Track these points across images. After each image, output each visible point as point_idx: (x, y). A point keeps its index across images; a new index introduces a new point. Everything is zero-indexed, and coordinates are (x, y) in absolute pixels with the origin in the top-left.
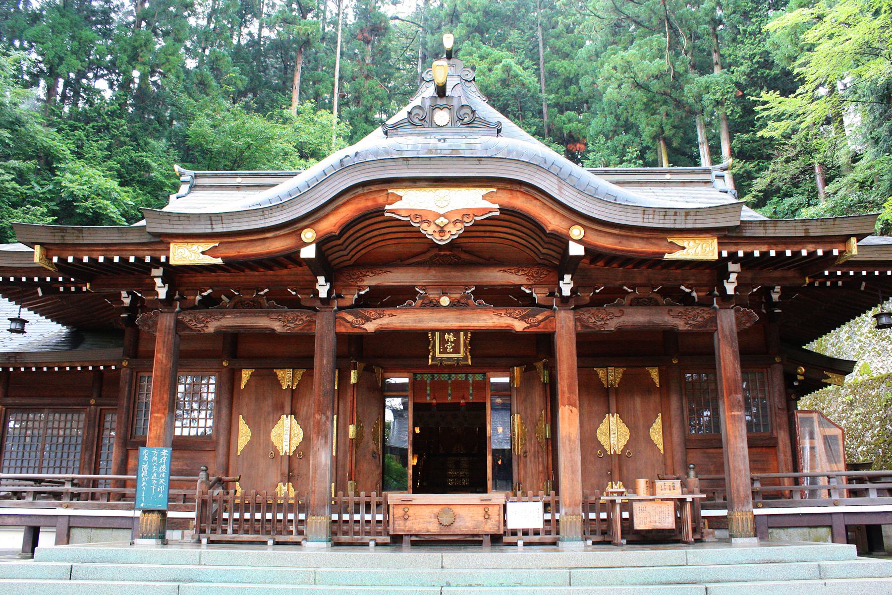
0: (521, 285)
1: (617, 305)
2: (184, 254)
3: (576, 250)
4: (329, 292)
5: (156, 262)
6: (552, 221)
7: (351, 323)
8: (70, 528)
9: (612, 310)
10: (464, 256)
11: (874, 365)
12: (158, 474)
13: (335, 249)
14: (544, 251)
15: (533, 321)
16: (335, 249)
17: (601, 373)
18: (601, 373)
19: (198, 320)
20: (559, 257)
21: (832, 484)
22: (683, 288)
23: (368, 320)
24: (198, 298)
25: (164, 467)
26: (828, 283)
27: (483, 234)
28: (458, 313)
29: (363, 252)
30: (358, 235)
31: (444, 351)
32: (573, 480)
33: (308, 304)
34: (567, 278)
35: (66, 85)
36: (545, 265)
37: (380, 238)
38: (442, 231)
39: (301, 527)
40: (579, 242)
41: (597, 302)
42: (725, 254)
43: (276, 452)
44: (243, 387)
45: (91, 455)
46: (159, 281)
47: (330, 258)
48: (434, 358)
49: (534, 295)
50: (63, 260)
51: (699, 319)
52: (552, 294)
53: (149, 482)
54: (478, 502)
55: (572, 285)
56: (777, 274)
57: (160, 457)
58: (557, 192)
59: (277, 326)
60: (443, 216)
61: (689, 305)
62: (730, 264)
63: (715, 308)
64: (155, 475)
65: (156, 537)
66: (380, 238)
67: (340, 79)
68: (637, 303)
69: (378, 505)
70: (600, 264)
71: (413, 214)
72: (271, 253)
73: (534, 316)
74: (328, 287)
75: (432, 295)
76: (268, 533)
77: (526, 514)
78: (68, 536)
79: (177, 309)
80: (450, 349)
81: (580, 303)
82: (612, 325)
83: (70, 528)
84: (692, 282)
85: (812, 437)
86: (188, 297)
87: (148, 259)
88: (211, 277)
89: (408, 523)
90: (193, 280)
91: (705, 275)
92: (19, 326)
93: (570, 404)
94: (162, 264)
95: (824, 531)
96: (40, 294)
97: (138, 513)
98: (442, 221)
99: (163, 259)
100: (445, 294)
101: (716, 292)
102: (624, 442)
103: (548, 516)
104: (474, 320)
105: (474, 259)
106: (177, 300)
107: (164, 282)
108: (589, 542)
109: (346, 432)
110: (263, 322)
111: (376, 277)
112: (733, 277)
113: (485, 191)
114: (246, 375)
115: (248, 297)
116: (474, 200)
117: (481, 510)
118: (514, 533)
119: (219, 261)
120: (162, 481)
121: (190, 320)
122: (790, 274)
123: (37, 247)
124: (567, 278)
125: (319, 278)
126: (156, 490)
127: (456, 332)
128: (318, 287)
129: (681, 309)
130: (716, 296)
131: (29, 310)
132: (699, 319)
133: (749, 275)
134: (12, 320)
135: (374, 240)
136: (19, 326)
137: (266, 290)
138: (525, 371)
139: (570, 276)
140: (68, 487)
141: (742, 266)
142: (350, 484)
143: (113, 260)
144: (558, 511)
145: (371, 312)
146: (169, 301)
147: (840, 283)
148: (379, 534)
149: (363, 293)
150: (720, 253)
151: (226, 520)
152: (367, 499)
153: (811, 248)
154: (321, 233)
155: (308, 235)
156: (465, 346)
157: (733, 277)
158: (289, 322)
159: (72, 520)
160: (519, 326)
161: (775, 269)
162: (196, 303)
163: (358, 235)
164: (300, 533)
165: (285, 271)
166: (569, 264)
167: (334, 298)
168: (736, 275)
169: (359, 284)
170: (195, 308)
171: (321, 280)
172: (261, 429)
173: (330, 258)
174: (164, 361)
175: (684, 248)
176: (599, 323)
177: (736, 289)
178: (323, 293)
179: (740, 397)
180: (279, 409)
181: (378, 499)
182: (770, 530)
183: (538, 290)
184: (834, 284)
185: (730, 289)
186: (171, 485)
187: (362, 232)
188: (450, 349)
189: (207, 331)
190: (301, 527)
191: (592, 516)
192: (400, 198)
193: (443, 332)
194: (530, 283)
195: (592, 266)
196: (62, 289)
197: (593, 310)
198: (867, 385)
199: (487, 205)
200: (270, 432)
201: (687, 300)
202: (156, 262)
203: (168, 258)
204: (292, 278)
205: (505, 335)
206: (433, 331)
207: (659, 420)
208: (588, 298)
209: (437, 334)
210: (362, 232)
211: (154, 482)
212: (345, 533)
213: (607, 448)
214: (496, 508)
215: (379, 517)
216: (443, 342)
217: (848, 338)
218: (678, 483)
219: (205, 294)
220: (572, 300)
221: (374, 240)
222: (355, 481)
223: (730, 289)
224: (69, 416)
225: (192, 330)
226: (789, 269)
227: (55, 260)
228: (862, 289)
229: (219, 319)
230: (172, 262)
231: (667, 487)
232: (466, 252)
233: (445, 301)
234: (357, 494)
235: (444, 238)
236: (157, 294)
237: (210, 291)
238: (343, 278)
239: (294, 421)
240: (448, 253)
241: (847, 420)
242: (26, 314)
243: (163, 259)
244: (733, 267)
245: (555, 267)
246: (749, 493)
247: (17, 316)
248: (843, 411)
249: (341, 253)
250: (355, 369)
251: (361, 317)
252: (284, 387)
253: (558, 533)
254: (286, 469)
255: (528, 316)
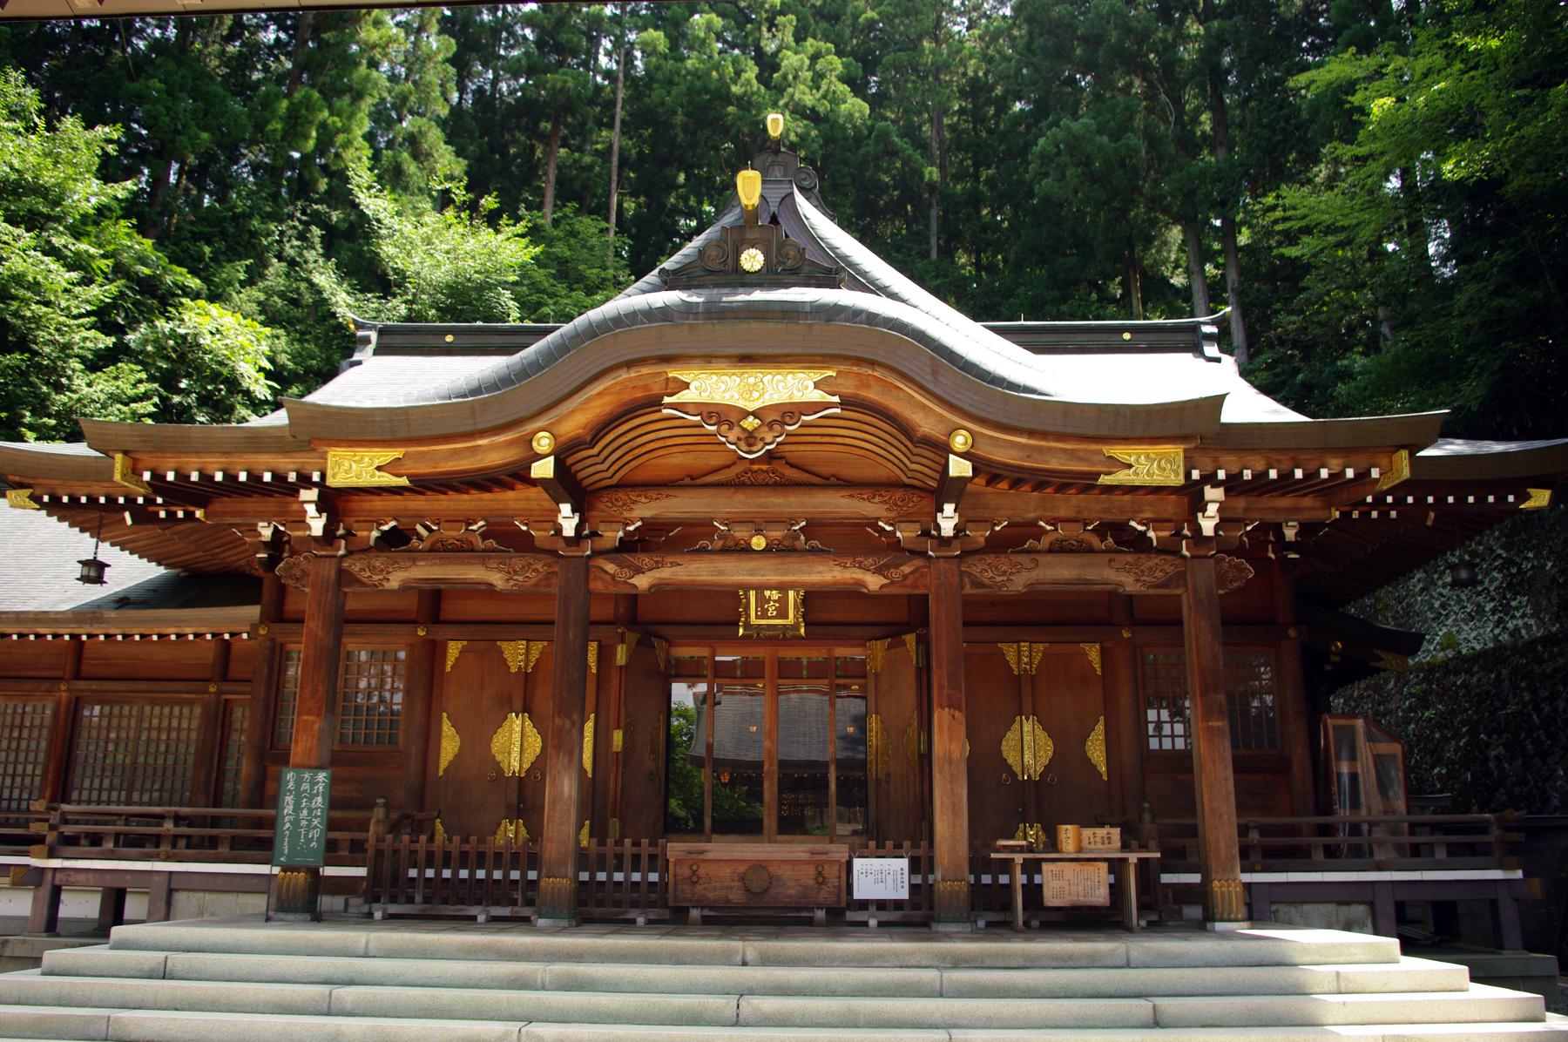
0: (878, 519)
1: (1028, 551)
2: (353, 468)
3: (959, 468)
4: (579, 528)
5: (304, 481)
6: (922, 423)
7: (613, 576)
8: (170, 892)
9: (1021, 558)
10: (791, 473)
11: (1464, 635)
12: (310, 811)
13: (588, 462)
14: (914, 467)
15: (895, 574)
16: (588, 462)
17: (1010, 652)
18: (1010, 652)
19: (373, 569)
20: (937, 476)
21: (1375, 836)
22: (1133, 523)
23: (639, 571)
24: (375, 534)
25: (320, 799)
26: (1374, 514)
27: (818, 439)
28: (778, 561)
29: (633, 464)
30: (623, 440)
31: (764, 615)
32: (954, 825)
33: (547, 546)
34: (949, 508)
35: (180, 173)
36: (915, 487)
37: (659, 444)
38: (750, 438)
39: (530, 894)
40: (964, 455)
41: (997, 545)
42: (1196, 475)
43: (500, 771)
44: (448, 669)
45: (210, 773)
46: (311, 509)
47: (581, 475)
48: (747, 626)
49: (899, 534)
50: (158, 477)
51: (1159, 574)
52: (926, 533)
53: (296, 823)
54: (805, 856)
55: (956, 520)
56: (1286, 502)
57: (313, 783)
58: (929, 377)
59: (497, 579)
60: (755, 414)
61: (1143, 552)
62: (1207, 489)
63: (1184, 557)
64: (305, 812)
65: (305, 911)
66: (659, 444)
67: (621, 166)
68: (1059, 548)
69: (653, 857)
70: (1003, 485)
71: (706, 410)
72: (485, 469)
73: (897, 566)
74: (576, 519)
75: (740, 533)
76: (478, 902)
77: (881, 877)
78: (169, 903)
79: (341, 552)
80: (772, 612)
81: (968, 548)
82: (1019, 582)
83: (170, 892)
84: (1148, 515)
85: (1353, 758)
86: (359, 534)
87: (292, 477)
88: (395, 503)
89: (699, 888)
90: (366, 506)
91: (1171, 506)
92: (94, 571)
93: (950, 706)
94: (316, 485)
95: (1359, 910)
96: (129, 522)
97: (276, 870)
98: (750, 423)
99: (316, 477)
100: (759, 532)
101: (1186, 532)
102: (1044, 761)
103: (918, 879)
104: (803, 572)
105: (805, 477)
106: (342, 537)
107: (320, 511)
108: (981, 924)
109: (609, 739)
110: (474, 573)
111: (653, 504)
112: (1212, 509)
113: (817, 375)
114: (454, 649)
115: (452, 533)
116: (795, 386)
117: (811, 871)
118: (864, 905)
119: (404, 481)
120: (316, 822)
121: (362, 570)
122: (1307, 502)
123: (119, 457)
124: (949, 508)
125: (562, 506)
126: (306, 835)
127: (783, 588)
128: (560, 520)
129: (1129, 558)
130: (1186, 537)
131: (113, 545)
132: (1159, 574)
133: (1240, 503)
134: (84, 563)
135: (649, 447)
136: (94, 571)
137: (481, 523)
138: (890, 646)
139: (952, 506)
140: (168, 825)
141: (1226, 492)
142: (614, 825)
143: (237, 477)
144: (932, 872)
145: (645, 560)
146: (329, 535)
147: (1393, 514)
148: (652, 905)
149: (631, 528)
150: (1188, 475)
151: (413, 879)
152: (635, 850)
153: (1336, 463)
154: (563, 439)
155: (543, 443)
156: (796, 607)
157: (1212, 509)
158: (516, 572)
159: (174, 877)
160: (874, 582)
161: (1283, 495)
162: (372, 542)
163: (623, 440)
164: (529, 902)
165: (511, 494)
166: (948, 489)
167: (587, 537)
168: (1216, 506)
169: (626, 514)
170: (368, 550)
171: (566, 508)
172: (477, 738)
173: (581, 475)
174: (320, 633)
175: (379, 468)
176: (999, 579)
177: (1217, 528)
178: (569, 529)
179: (1221, 698)
180: (505, 706)
181: (651, 850)
182: (1274, 908)
183: (903, 525)
184: (1384, 515)
185: (1208, 525)
186: (332, 825)
187: (630, 436)
188: (772, 612)
189: (387, 586)
190: (530, 894)
191: (986, 879)
192: (687, 386)
193: (760, 588)
194: (893, 514)
195: (989, 489)
196: (162, 514)
197: (990, 559)
198: (1447, 668)
199: (818, 396)
200: (490, 740)
201: (1139, 543)
202: (304, 481)
203: (323, 476)
204: (522, 505)
205: (853, 593)
206: (747, 588)
207: (1100, 727)
208: (982, 540)
209: (752, 594)
210: (630, 436)
211: (304, 823)
212: (600, 903)
213: (1017, 769)
214: (836, 867)
215: (654, 877)
216: (762, 601)
217: (1423, 590)
218: (1116, 833)
219: (386, 528)
220: (956, 543)
221: (649, 447)
222: (621, 819)
223: (1208, 525)
224: (177, 710)
225: (364, 585)
226: (1305, 495)
227: (147, 476)
228: (1429, 523)
229: (406, 569)
230: (331, 482)
231: (1098, 839)
232: (792, 466)
233: (759, 543)
234: (619, 843)
235: (754, 449)
236: (309, 528)
237: (393, 523)
238: (601, 506)
239: (528, 722)
240: (764, 467)
241: (1417, 724)
242: (107, 552)
243: (316, 477)
244: (1213, 494)
245: (930, 491)
246: (1236, 851)
247: (91, 557)
248: (1411, 709)
249: (598, 468)
250: (622, 642)
251: (628, 567)
252: (514, 670)
253: (931, 908)
254: (514, 799)
255: (887, 566)
